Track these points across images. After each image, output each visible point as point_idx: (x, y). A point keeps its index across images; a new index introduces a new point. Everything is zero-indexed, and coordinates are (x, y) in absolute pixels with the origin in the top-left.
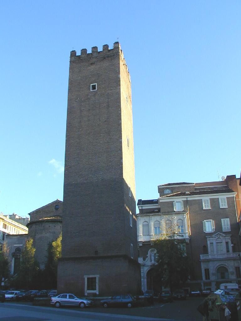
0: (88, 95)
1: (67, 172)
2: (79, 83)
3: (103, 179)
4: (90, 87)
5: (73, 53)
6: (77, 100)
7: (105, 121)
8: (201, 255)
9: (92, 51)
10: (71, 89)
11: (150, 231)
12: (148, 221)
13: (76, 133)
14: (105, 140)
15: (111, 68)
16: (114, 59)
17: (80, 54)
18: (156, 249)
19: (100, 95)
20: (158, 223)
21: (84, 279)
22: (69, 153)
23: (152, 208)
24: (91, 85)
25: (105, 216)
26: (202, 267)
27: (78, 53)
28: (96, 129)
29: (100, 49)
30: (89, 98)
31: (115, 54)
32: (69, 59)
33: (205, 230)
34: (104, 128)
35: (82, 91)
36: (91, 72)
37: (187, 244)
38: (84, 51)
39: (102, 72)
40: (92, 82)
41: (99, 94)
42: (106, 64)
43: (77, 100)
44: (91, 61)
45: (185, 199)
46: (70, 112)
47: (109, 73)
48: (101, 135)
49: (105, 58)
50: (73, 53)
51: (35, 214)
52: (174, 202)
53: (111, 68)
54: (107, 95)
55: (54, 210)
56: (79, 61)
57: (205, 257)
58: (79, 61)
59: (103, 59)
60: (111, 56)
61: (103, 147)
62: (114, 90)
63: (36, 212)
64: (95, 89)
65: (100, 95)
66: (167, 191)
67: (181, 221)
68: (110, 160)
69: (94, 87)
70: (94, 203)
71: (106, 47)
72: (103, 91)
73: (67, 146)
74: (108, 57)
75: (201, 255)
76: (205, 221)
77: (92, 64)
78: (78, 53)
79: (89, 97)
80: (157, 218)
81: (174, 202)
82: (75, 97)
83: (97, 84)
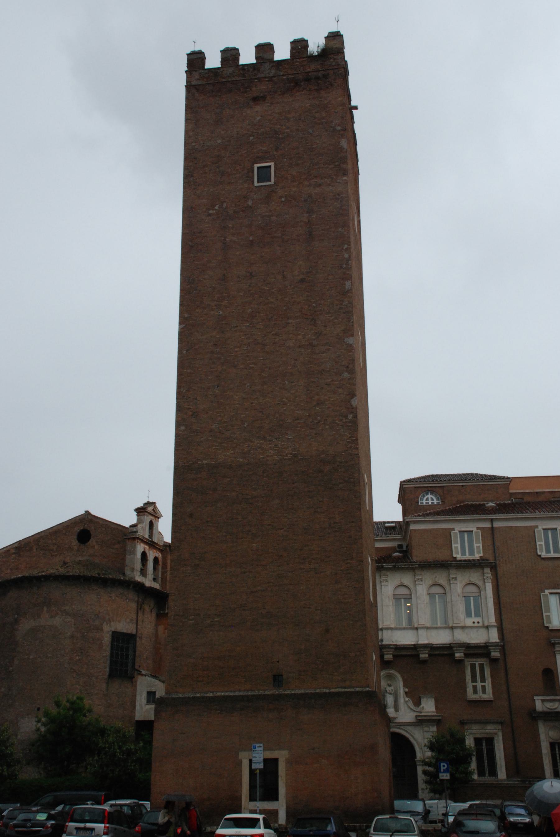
0: (246, 198)
1: (182, 428)
2: (218, 156)
3: (296, 456)
4: (253, 172)
5: (196, 60)
6: (211, 212)
7: (302, 281)
8: (535, 698)
9: (257, 58)
10: (192, 176)
11: (414, 613)
12: (411, 586)
13: (212, 313)
14: (299, 337)
15: (317, 115)
16: (332, 85)
17: (219, 65)
18: (399, 672)
19: (283, 199)
20: (441, 591)
21: (240, 763)
22: (189, 371)
23: (402, 552)
24: (256, 166)
25: (302, 566)
26: (542, 737)
27: (213, 61)
28: (272, 302)
29: (282, 53)
30: (251, 207)
31: (331, 73)
32: (182, 80)
33: (549, 621)
34: (299, 303)
35: (229, 183)
36: (255, 125)
37: (494, 661)
38: (230, 55)
39: (288, 128)
40: (258, 157)
41: (281, 197)
42: (301, 101)
43: (211, 212)
44: (259, 89)
45: (487, 525)
46: (192, 247)
47: (310, 131)
48: (290, 321)
49: (297, 84)
50: (196, 60)
51: (13, 556)
52: (452, 532)
53: (317, 115)
54: (305, 201)
55: (75, 543)
56: (222, 92)
57: (551, 704)
58: (222, 92)
59: (293, 84)
60: (317, 78)
61: (296, 360)
62: (329, 185)
63: (16, 548)
64: (270, 180)
65: (283, 199)
66: (429, 500)
67: (472, 589)
68: (316, 397)
69: (264, 174)
70: (270, 525)
71: (299, 46)
72: (294, 189)
73: (185, 352)
74: (308, 80)
75: (535, 698)
76: (547, 592)
77: (256, 100)
78: (213, 61)
79: (250, 203)
80: (407, 579)
81: (536, 529)
82: (205, 201)
83: (272, 164)
